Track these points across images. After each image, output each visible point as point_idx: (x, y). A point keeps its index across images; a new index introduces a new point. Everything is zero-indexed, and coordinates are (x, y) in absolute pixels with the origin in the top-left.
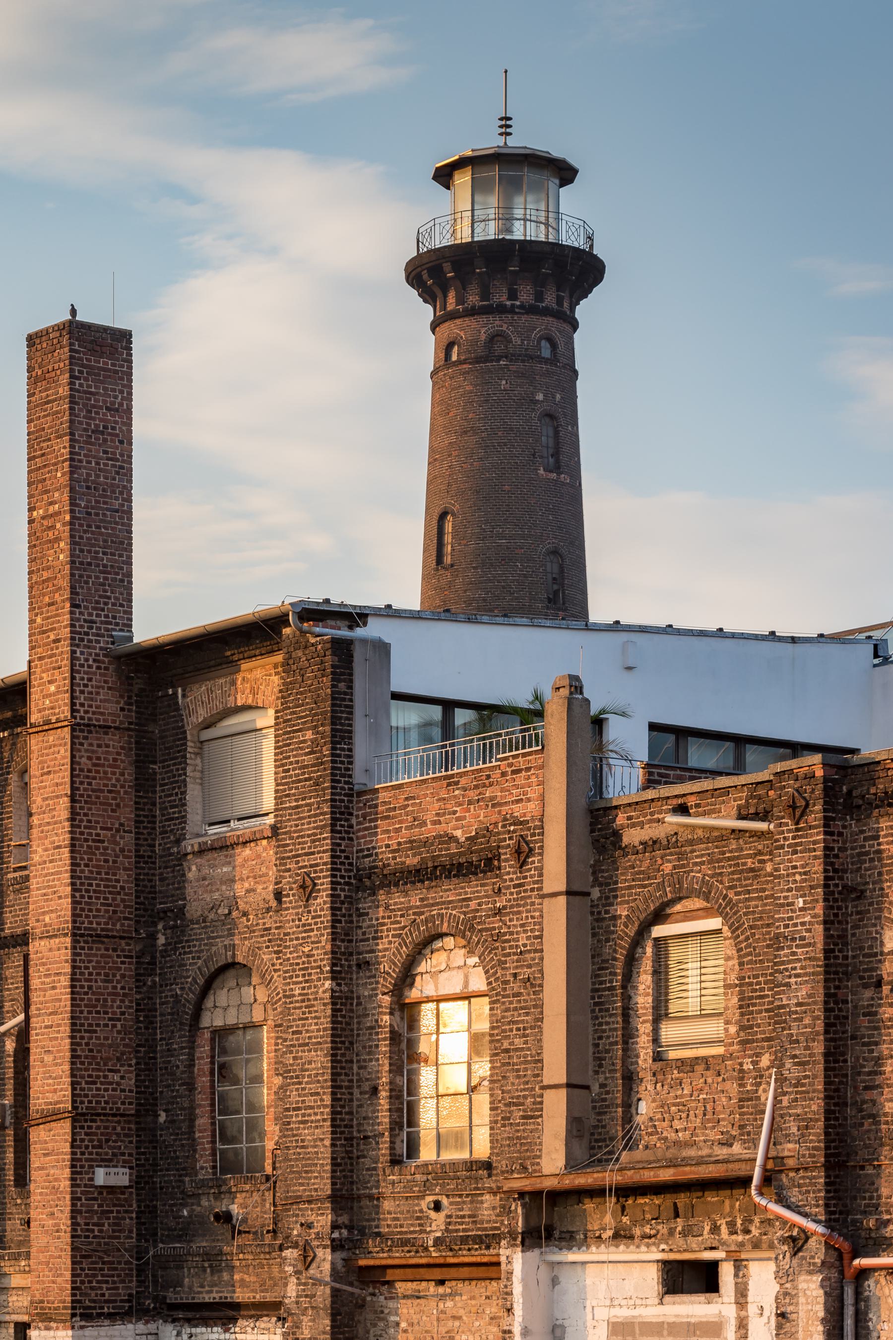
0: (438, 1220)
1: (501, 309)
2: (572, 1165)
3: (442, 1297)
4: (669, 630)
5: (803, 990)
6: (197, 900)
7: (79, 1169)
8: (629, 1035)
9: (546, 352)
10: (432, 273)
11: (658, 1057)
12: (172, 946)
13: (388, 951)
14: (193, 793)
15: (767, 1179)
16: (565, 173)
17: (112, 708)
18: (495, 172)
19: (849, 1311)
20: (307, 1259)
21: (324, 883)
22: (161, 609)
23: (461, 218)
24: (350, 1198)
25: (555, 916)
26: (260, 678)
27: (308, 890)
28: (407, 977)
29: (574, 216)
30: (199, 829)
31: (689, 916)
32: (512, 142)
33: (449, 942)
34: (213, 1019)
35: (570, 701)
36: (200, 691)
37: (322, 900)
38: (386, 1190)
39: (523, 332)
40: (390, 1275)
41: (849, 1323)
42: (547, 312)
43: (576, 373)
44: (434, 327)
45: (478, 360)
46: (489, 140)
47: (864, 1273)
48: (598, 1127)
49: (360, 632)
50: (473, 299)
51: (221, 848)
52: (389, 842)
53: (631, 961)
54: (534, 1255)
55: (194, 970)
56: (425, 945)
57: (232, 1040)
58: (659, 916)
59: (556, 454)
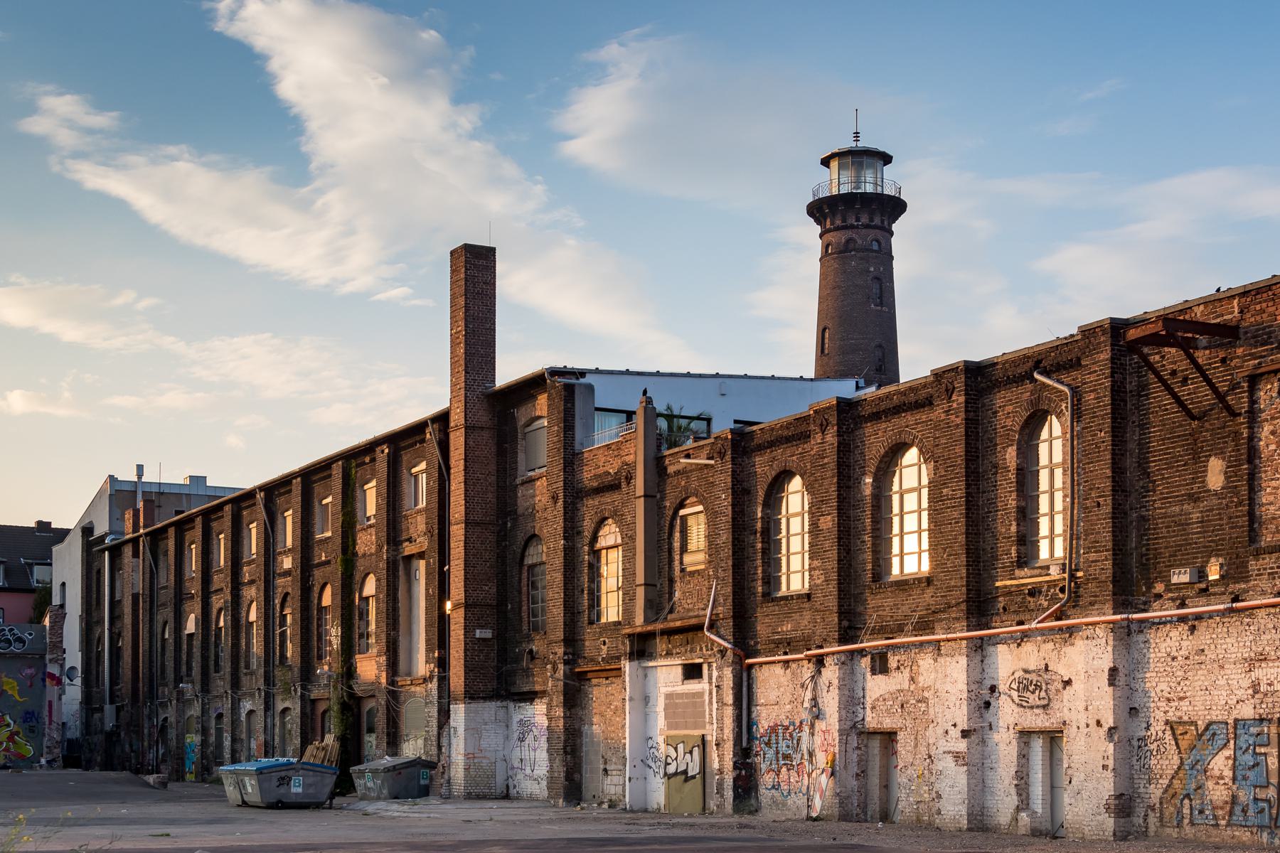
0: (604, 648)
1: (852, 227)
2: (647, 621)
3: (607, 685)
4: (628, 372)
5: (725, 537)
6: (522, 505)
7: (468, 630)
8: (671, 561)
9: (875, 247)
10: (820, 210)
11: (683, 570)
12: (513, 527)
13: (588, 525)
14: (521, 457)
15: (711, 627)
16: (887, 159)
17: (485, 419)
18: (850, 159)
19: (745, 684)
20: (555, 669)
21: (561, 495)
22: (508, 371)
23: (834, 182)
24: (572, 640)
25: (640, 504)
26: (542, 403)
27: (555, 499)
28: (595, 538)
29: (892, 180)
30: (523, 473)
31: (693, 505)
32: (860, 144)
33: (610, 521)
34: (529, 561)
35: (645, 408)
36: (523, 410)
37: (560, 503)
38: (587, 637)
39: (864, 238)
40: (589, 675)
41: (745, 689)
42: (875, 227)
43: (892, 258)
44: (821, 236)
45: (840, 252)
46: (849, 144)
47: (751, 666)
48: (658, 601)
49: (582, 380)
52: (587, 476)
53: (672, 527)
54: (635, 663)
55: (521, 538)
56: (601, 523)
57: (537, 569)
58: (682, 505)
59: (881, 297)
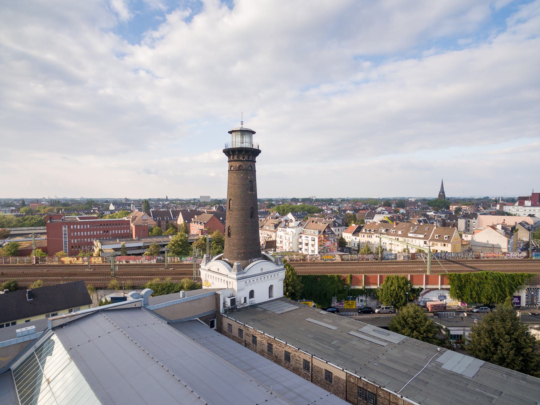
1: (241, 161)
9: (250, 169)
10: (228, 152)
16: (254, 133)
23: (237, 142)
29: (256, 142)
42: (250, 161)
44: (229, 162)
46: (238, 127)
50: (236, 158)
51: (61, 326)
